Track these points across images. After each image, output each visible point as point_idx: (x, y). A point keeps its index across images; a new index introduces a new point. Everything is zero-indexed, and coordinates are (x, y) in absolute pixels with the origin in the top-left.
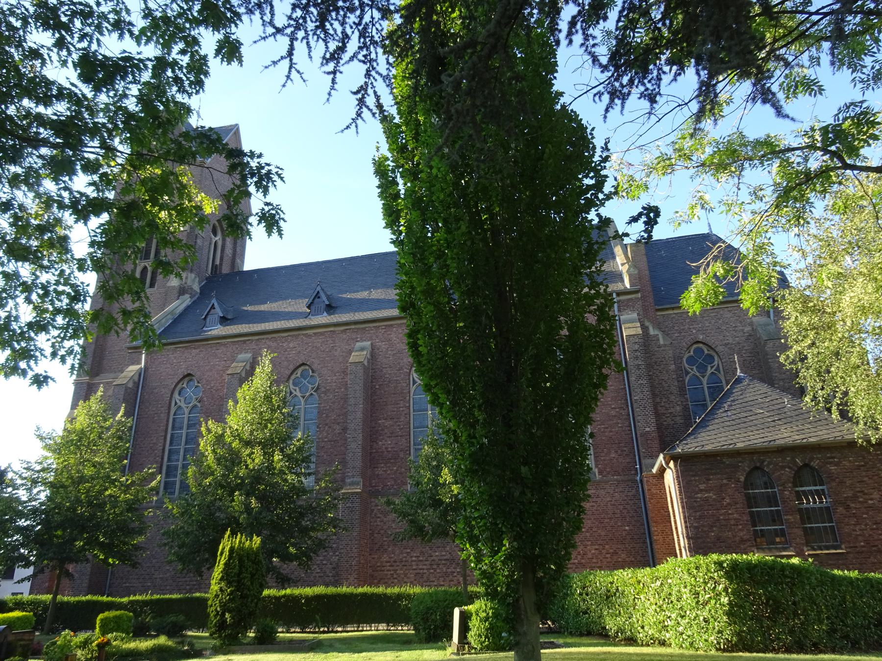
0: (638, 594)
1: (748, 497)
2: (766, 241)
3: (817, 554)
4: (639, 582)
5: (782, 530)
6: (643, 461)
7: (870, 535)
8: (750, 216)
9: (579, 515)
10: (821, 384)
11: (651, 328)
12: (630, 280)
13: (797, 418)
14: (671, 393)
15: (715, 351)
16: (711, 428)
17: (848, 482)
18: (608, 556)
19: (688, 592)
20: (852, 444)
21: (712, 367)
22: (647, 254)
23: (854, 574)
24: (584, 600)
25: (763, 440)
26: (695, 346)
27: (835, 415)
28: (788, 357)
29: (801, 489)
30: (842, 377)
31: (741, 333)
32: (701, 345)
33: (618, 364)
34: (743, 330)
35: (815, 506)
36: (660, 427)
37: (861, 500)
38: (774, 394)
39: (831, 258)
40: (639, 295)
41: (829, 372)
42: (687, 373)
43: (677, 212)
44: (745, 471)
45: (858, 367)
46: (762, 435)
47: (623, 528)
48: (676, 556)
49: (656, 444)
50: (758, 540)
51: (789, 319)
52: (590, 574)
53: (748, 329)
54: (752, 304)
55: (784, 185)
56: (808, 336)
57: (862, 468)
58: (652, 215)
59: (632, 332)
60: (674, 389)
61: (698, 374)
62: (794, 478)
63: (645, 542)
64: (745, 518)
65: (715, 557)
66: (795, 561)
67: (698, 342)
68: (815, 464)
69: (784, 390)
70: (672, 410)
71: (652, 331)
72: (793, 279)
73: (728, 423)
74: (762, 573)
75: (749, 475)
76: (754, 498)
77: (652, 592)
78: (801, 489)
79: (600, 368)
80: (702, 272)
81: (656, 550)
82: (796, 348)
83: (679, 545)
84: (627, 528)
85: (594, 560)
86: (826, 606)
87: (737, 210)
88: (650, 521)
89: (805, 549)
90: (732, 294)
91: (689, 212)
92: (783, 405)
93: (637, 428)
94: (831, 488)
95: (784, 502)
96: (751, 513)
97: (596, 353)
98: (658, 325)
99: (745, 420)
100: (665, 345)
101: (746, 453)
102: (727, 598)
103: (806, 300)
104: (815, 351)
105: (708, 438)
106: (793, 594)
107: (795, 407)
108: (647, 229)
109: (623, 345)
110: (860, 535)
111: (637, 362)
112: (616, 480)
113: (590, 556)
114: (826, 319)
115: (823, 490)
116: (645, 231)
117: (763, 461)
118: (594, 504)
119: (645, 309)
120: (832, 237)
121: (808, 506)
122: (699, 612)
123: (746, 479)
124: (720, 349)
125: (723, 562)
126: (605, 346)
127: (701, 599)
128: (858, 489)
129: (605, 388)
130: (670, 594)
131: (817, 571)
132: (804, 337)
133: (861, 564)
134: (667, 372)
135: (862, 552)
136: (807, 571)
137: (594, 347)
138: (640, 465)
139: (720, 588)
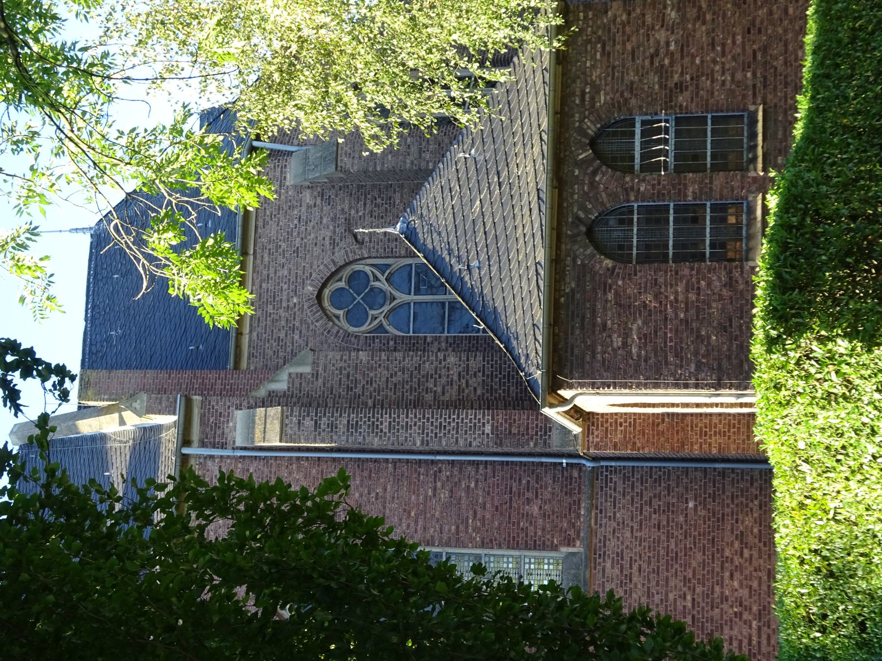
0: (826, 512)
1: (645, 259)
2: (123, 141)
3: (765, 155)
4: (802, 506)
5: (714, 208)
6: (554, 449)
7: (734, 58)
8: (66, 159)
9: (650, 625)
10: (437, 89)
11: (274, 386)
12: (159, 412)
13: (499, 141)
14: (418, 368)
15: (341, 268)
16: (499, 304)
17: (632, 77)
18: (746, 554)
19: (824, 413)
20: (560, 58)
21: (376, 279)
22: (111, 368)
23: (803, 103)
24: (836, 625)
25: (535, 212)
26: (326, 303)
27: (500, 76)
28: (375, 137)
29: (637, 160)
30: (430, 51)
31: (316, 212)
32: (327, 292)
33: (330, 486)
34: (309, 207)
35: (672, 142)
36: (487, 403)
37: (667, 62)
38: (447, 174)
39: (188, 25)
40: (197, 399)
41: (415, 70)
42: (380, 328)
43: (22, 299)
44: (592, 256)
45: (412, 19)
46: (526, 210)
47: (691, 513)
48: (753, 416)
49: (521, 417)
50: (730, 255)
51: (298, 121)
52: (781, 602)
53: (307, 197)
54: (250, 189)
55: (10, 85)
56: (337, 94)
57: (607, 48)
58: (9, 358)
59: (274, 427)
60: (411, 360)
61: (386, 308)
62: (614, 169)
63: (723, 473)
64: (686, 272)
65: (757, 349)
66: (773, 201)
67: (319, 297)
68: (591, 128)
69: (441, 152)
70: (454, 372)
71: (281, 385)
72: (216, 99)
73: (495, 269)
74: (793, 266)
75: (601, 249)
76: (648, 247)
77: (824, 484)
78: (637, 160)
79: (333, 526)
80: (167, 273)
81: (740, 454)
82: (358, 118)
83: (732, 405)
84: (691, 505)
85: (755, 584)
86: (861, 162)
87: (44, 182)
88: (680, 455)
89: (752, 174)
90: (218, 224)
91: (28, 275)
92: (470, 163)
93: (483, 449)
94: (641, 107)
95: (660, 196)
96: (677, 258)
97: (298, 529)
98: (271, 370)
99: (491, 236)
100: (315, 364)
101: (558, 248)
102: (839, 341)
103: (264, 84)
104: (369, 87)
105: (519, 312)
106: (835, 216)
107: (478, 142)
108: (40, 374)
109: (299, 449)
110: (733, 76)
111: (342, 428)
112: (589, 511)
113: (745, 593)
114: (309, 55)
115: (643, 123)
116: (44, 379)
117: (577, 218)
118: (635, 567)
119: (229, 391)
120: (148, 15)
121: (671, 154)
122: (866, 399)
123: (608, 256)
124: (340, 257)
125: (767, 336)
126: (285, 508)
127: (839, 390)
128: (647, 62)
129: (379, 521)
130: (827, 448)
131: (794, 166)
132: (339, 101)
133: (786, 84)
134: (371, 369)
135: (765, 78)
136: (792, 184)
137: (283, 531)
138: (562, 456)
139: (819, 351)
